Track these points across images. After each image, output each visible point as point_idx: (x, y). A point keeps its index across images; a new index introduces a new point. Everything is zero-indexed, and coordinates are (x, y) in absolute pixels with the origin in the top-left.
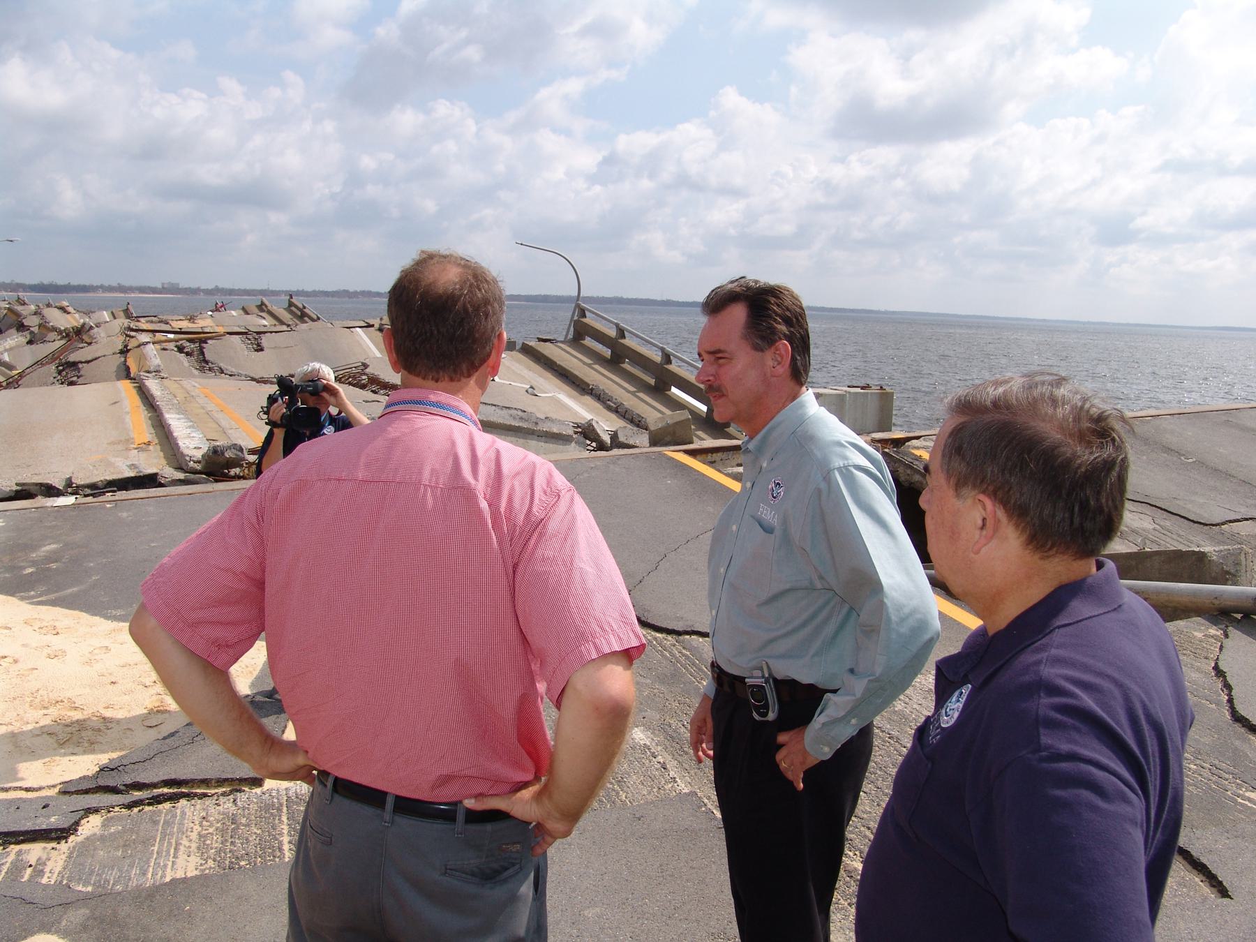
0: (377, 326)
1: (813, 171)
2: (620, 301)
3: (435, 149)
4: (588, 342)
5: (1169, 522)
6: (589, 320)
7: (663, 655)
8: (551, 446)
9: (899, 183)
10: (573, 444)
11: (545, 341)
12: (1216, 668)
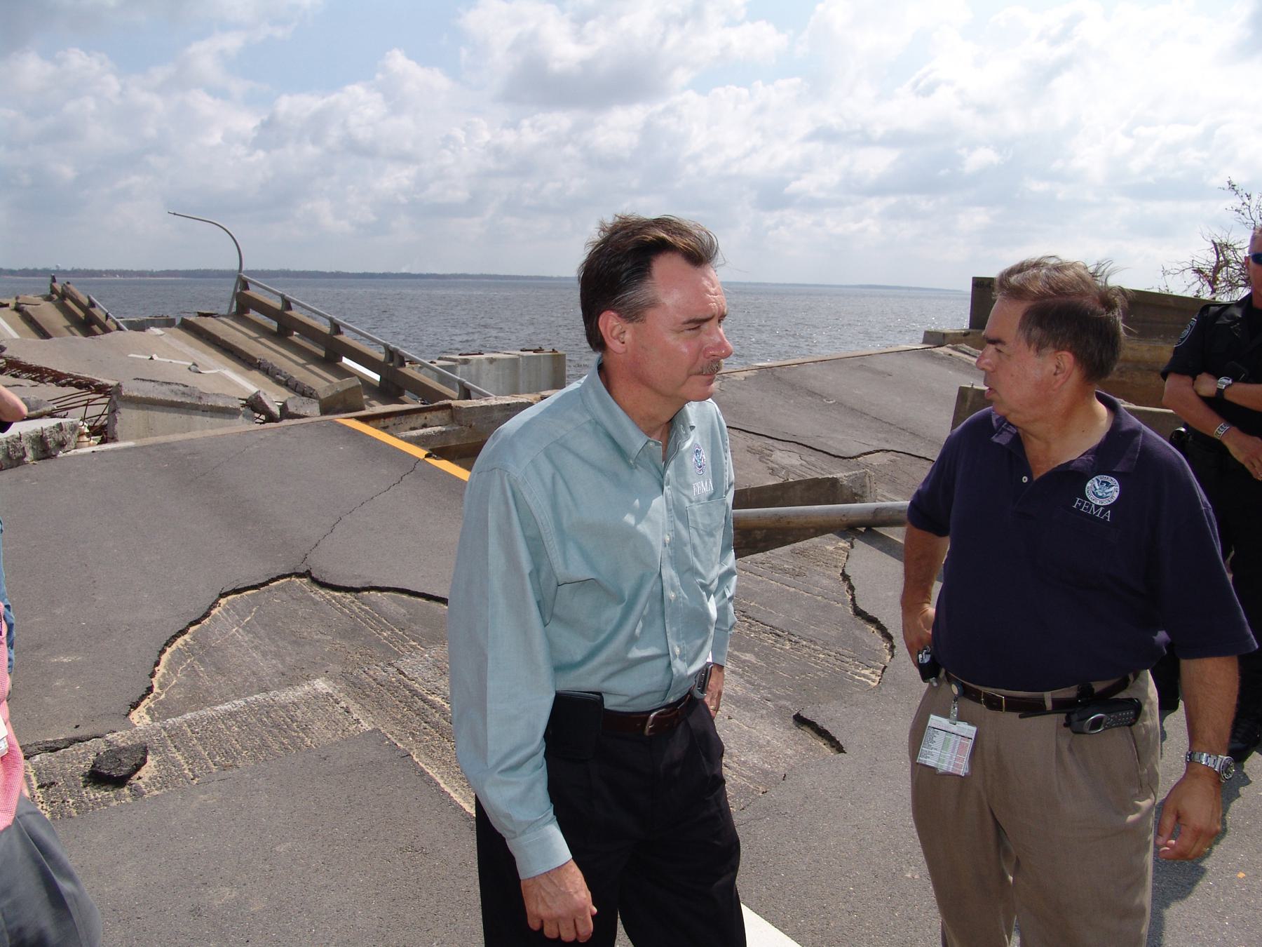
0: (12, 305)
1: (486, 136)
2: (286, 274)
3: (71, 107)
4: (253, 315)
5: (813, 458)
6: (253, 292)
7: (342, 612)
8: (217, 421)
9: (569, 150)
10: (241, 417)
11: (206, 315)
12: (843, 574)
